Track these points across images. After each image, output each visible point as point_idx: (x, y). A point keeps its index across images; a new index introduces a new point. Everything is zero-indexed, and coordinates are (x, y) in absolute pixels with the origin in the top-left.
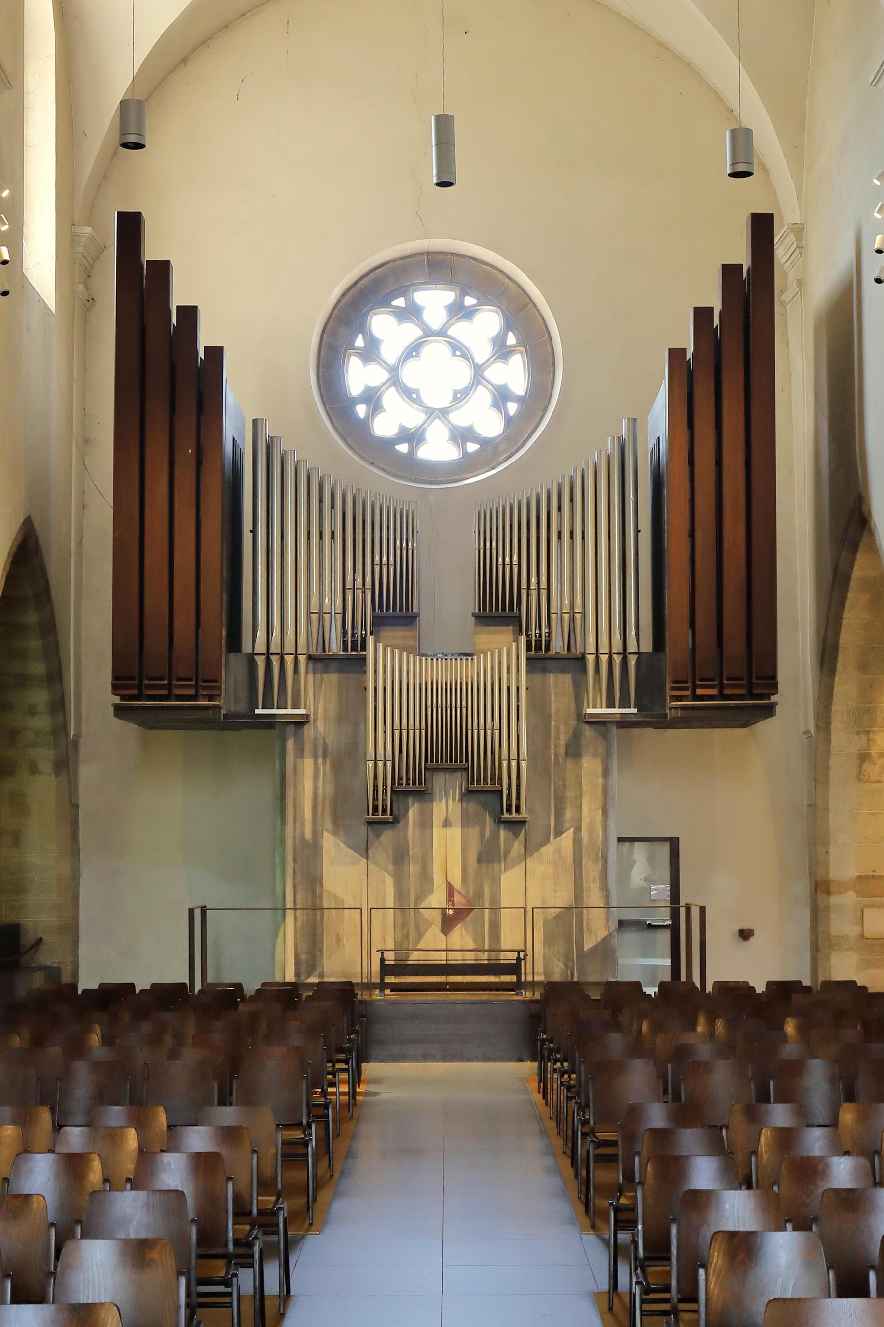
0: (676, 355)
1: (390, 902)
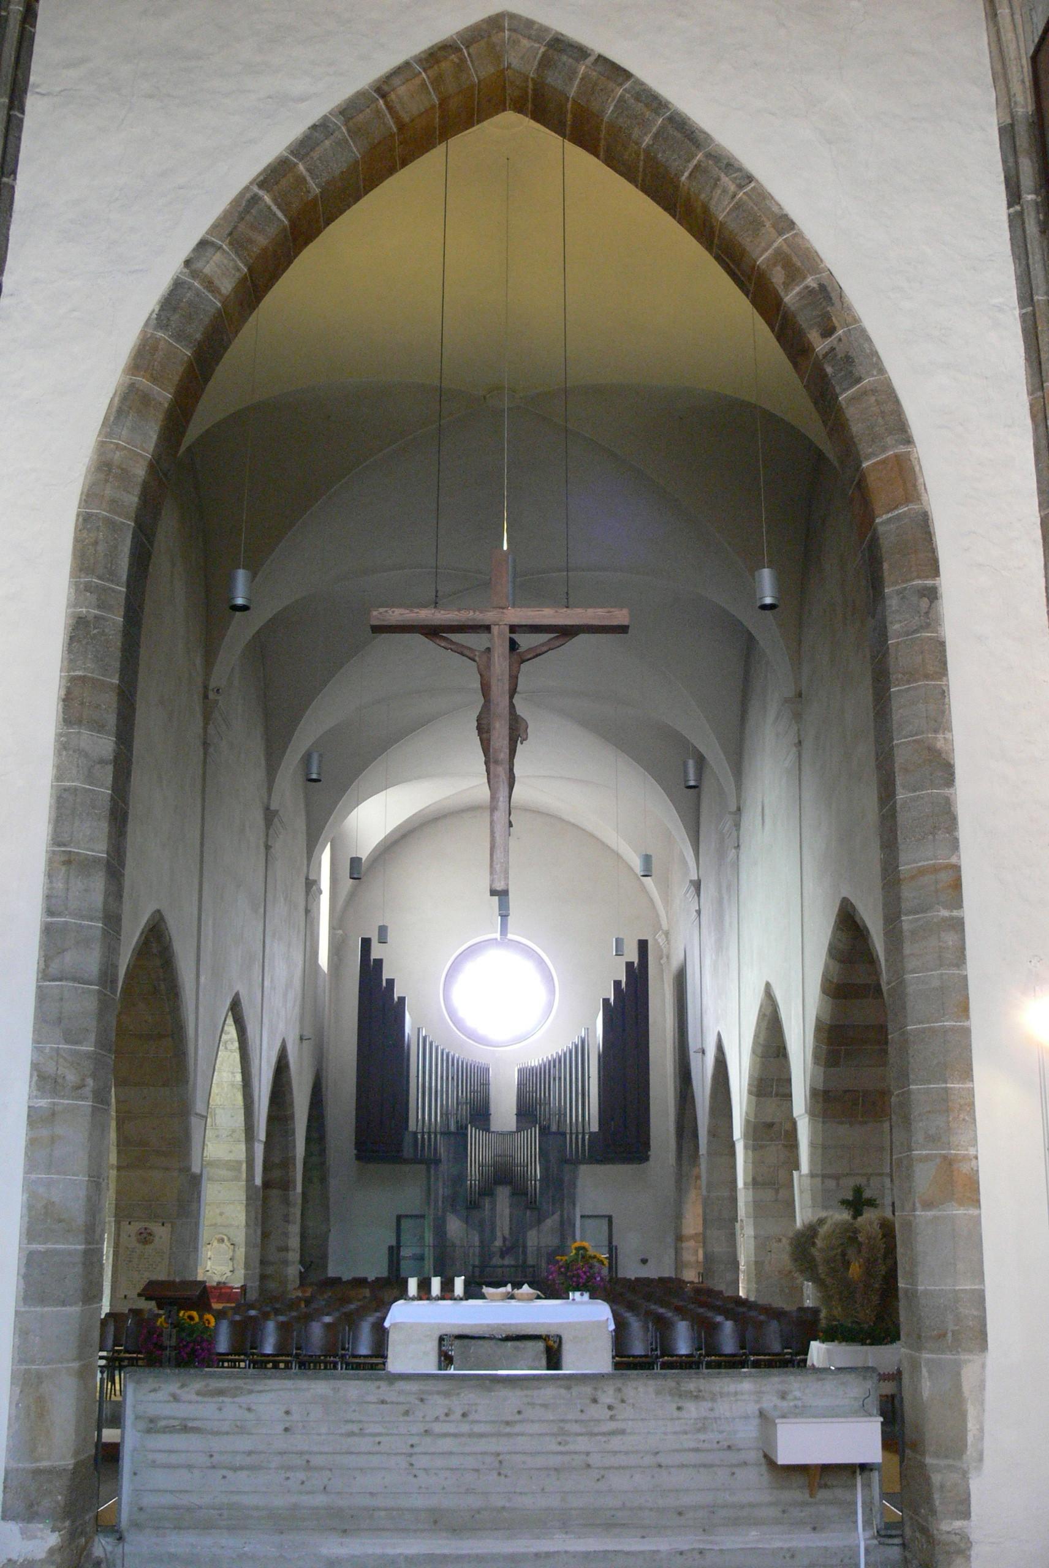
0: (606, 1001)
1: (477, 1244)
